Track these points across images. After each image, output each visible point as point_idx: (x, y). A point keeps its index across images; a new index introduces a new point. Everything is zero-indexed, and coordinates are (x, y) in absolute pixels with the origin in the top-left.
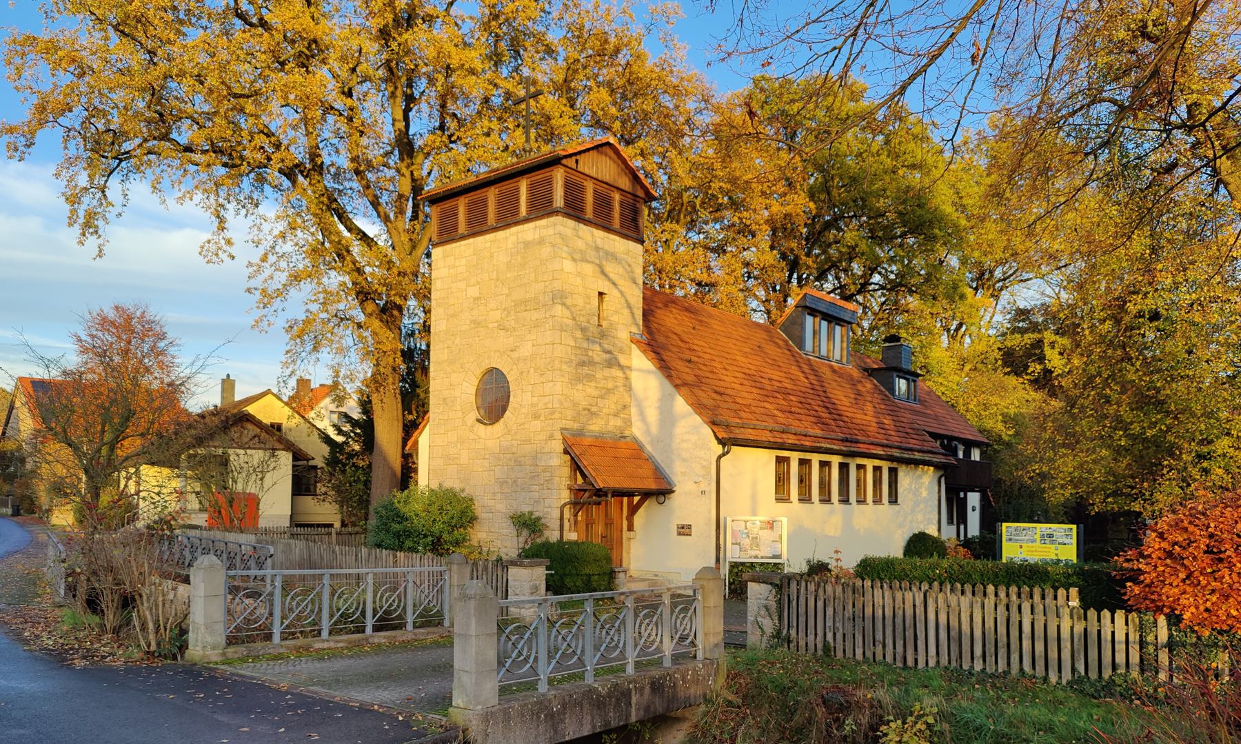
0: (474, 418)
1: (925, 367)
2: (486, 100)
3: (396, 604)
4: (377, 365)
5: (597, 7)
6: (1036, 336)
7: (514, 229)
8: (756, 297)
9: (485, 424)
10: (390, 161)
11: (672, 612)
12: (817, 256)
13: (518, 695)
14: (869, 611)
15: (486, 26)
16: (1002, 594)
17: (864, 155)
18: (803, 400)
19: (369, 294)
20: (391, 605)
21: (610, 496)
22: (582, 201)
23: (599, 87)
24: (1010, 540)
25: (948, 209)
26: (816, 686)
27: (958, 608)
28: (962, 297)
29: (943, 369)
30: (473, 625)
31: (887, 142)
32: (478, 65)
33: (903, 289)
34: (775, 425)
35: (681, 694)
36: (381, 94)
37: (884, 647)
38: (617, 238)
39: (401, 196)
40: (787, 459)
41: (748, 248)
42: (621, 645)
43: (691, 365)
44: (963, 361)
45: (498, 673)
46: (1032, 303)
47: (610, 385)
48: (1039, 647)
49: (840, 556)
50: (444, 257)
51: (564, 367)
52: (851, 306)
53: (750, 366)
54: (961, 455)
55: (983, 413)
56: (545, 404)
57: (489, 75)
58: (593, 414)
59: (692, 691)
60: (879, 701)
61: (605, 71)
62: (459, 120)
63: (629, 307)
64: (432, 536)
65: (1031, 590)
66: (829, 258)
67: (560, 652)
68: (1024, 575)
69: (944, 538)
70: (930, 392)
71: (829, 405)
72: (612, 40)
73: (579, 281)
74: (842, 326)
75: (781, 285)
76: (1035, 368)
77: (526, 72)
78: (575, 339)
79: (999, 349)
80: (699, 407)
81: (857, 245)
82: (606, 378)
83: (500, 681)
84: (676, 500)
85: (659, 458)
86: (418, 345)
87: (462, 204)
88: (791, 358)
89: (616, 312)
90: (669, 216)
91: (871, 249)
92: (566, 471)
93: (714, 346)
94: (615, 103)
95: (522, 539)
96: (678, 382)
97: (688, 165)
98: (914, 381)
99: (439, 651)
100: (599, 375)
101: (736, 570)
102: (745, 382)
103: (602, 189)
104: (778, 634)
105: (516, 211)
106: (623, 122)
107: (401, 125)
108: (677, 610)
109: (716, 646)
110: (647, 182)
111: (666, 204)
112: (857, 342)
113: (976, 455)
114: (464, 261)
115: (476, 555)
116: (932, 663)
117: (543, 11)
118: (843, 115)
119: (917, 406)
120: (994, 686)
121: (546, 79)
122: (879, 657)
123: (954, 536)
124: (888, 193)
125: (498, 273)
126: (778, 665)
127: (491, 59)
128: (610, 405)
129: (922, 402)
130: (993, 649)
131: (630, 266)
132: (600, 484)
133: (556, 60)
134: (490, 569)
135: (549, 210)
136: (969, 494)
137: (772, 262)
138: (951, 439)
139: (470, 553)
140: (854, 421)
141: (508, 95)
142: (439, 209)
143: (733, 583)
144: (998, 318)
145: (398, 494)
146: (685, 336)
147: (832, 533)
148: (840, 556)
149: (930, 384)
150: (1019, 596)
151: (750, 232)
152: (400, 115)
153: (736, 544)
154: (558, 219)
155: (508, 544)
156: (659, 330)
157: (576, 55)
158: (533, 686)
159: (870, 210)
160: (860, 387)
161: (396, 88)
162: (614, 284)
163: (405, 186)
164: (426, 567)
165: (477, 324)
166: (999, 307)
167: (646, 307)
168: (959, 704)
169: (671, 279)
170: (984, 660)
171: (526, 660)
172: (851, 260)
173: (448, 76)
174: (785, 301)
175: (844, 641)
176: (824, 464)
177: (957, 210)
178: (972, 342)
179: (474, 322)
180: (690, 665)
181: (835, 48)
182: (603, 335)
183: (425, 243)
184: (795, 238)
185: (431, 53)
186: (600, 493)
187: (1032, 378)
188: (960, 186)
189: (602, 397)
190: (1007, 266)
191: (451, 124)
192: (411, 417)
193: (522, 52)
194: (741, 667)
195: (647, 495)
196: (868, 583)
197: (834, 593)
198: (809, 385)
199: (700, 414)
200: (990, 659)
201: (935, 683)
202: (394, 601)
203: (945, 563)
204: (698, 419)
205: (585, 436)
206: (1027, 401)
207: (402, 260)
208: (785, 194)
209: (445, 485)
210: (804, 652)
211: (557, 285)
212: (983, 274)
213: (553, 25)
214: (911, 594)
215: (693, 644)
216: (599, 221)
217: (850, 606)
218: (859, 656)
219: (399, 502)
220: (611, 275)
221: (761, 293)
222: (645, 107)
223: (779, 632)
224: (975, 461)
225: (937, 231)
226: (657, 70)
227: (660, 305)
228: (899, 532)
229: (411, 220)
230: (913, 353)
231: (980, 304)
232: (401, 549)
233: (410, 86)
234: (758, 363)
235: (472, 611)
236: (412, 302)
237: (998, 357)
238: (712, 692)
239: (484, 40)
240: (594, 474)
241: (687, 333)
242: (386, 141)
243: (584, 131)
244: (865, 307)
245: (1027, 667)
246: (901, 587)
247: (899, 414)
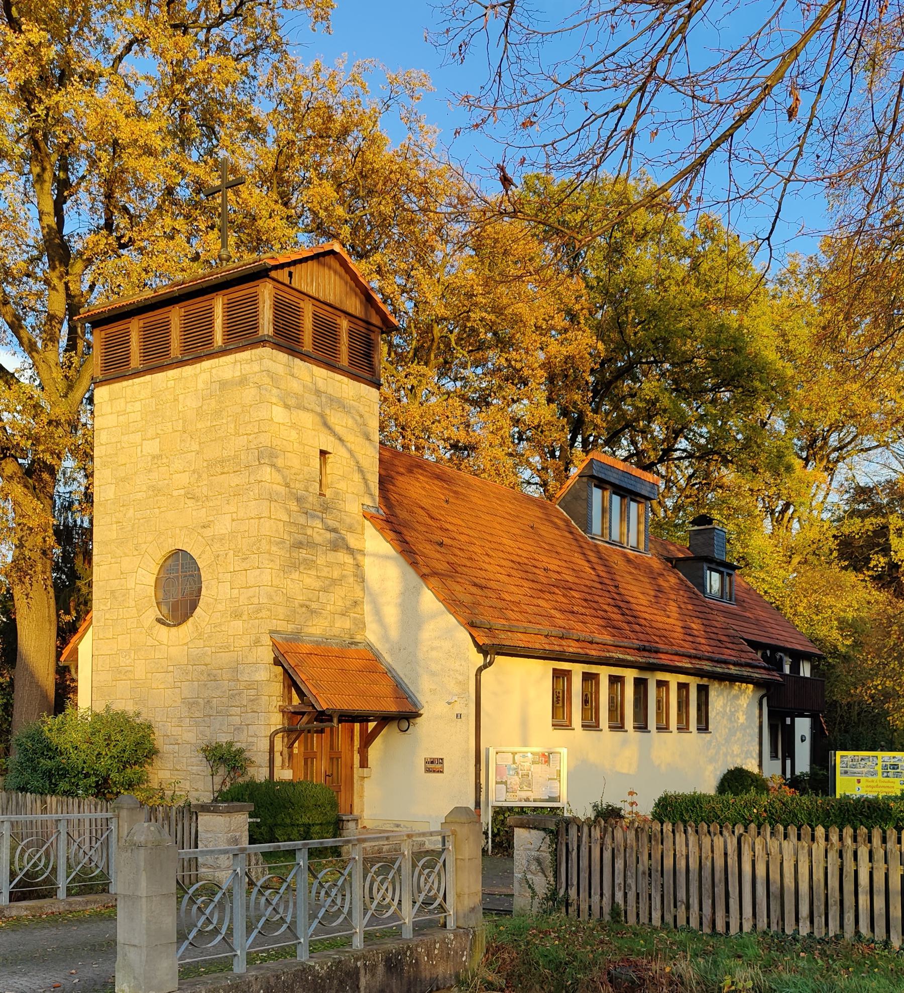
0: (153, 617)
1: (743, 558)
2: (170, 191)
3: (42, 864)
4: (20, 546)
5: (318, 71)
6: (880, 520)
7: (206, 364)
8: (529, 464)
9: (168, 625)
10: (37, 270)
11: (414, 866)
12: (607, 413)
13: (205, 978)
14: (668, 863)
15: (169, 92)
16: (834, 838)
17: (666, 283)
18: (588, 597)
19: (8, 449)
20: (35, 865)
21: (335, 720)
22: (298, 328)
23: (321, 179)
24: (846, 772)
25: (771, 355)
26: (601, 960)
27: (779, 856)
28: (789, 468)
29: (767, 561)
30: (144, 883)
31: (695, 267)
32: (157, 142)
33: (716, 457)
34: (552, 628)
35: (426, 974)
36: (24, 178)
37: (688, 908)
38: (345, 379)
39: (51, 317)
40: (567, 673)
41: (518, 400)
42: (346, 910)
43: (442, 550)
44: (791, 552)
45: (178, 949)
46: (876, 479)
47: (336, 574)
48: (879, 903)
49: (635, 798)
50: (111, 400)
51: (274, 549)
52: (649, 477)
53: (520, 552)
54: (787, 670)
55: (814, 617)
56: (249, 598)
57: (172, 157)
58: (313, 612)
59: (440, 970)
60: (680, 976)
61: (329, 159)
62: (131, 217)
63: (361, 470)
64: (96, 775)
65: (870, 832)
66: (622, 416)
67: (263, 919)
68: (861, 814)
69: (766, 775)
70: (750, 590)
71: (622, 604)
72: (339, 117)
73: (294, 434)
74: (639, 502)
75: (561, 449)
76: (879, 561)
77: (222, 154)
78: (289, 512)
79: (834, 536)
80: (452, 604)
81: (657, 400)
82: (329, 565)
83: (181, 959)
84: (422, 725)
85: (401, 671)
86: (79, 522)
87: (135, 328)
88: (574, 543)
89: (344, 477)
90: (415, 355)
91: (675, 405)
92: (277, 687)
93: (473, 526)
94: (342, 201)
95: (218, 779)
96: (426, 571)
97: (440, 289)
98: (730, 575)
99: (101, 924)
100: (321, 561)
101: (501, 817)
102: (513, 572)
103: (324, 312)
104: (552, 896)
105: (209, 339)
106: (355, 230)
107: (51, 220)
108: (420, 864)
109: (473, 910)
110: (387, 309)
111: (412, 340)
112: (659, 525)
113: (806, 670)
114: (138, 406)
115: (155, 801)
116: (747, 927)
117: (244, 72)
118: (639, 229)
119: (734, 607)
120: (823, 953)
121: (250, 167)
122: (682, 921)
123: (780, 772)
124: (697, 333)
125: (185, 421)
126: (553, 935)
127: (175, 135)
128: (335, 600)
129: (739, 602)
130: (823, 907)
131: (361, 416)
132: (323, 705)
133: (264, 141)
134: (173, 818)
135: (254, 338)
136: (796, 719)
137: (549, 418)
138: (775, 649)
139: (148, 798)
140: (654, 624)
141: (199, 187)
142: (103, 334)
143: (498, 834)
144: (834, 497)
145: (50, 720)
146: (435, 512)
147: (625, 771)
148: (635, 798)
149: (749, 580)
150: (855, 840)
151: (520, 378)
152: (49, 207)
153: (501, 783)
154: (266, 352)
155: (200, 785)
156: (400, 504)
157: (290, 136)
158: (226, 965)
159: (674, 354)
160: (661, 581)
161: (44, 169)
162: (340, 439)
163: (58, 304)
164: (87, 814)
165: (156, 490)
166: (835, 484)
167: (383, 473)
168: (780, 976)
169: (418, 438)
170: (812, 922)
171: (216, 931)
172: (650, 419)
173: (115, 156)
174: (567, 469)
175: (638, 903)
176: (615, 680)
177: (782, 357)
178: (802, 527)
179: (153, 488)
180: (439, 935)
181: (617, 107)
182: (326, 508)
183: (85, 382)
184: (579, 388)
185: (91, 122)
186: (323, 716)
187: (875, 574)
188: (786, 326)
189: (325, 590)
190: (845, 431)
191: (121, 221)
192: (68, 618)
193: (217, 128)
194: (505, 938)
195: (385, 720)
196: (667, 827)
197: (625, 841)
198: (596, 578)
199: (454, 613)
200: (819, 920)
201: (750, 952)
202: (40, 859)
203: (764, 800)
204: (452, 619)
205: (303, 641)
206: (869, 603)
207: (53, 404)
208: (566, 330)
209: (113, 707)
210: (587, 918)
211: (265, 440)
212: (815, 441)
213: (259, 94)
214: (722, 839)
215: (442, 909)
216: (319, 355)
217: (646, 857)
218: (657, 921)
219: (50, 730)
220: (338, 429)
221: (536, 460)
222: (382, 208)
223: (555, 892)
225: (757, 384)
226: (399, 160)
227: (402, 470)
228: (710, 768)
229: (66, 351)
230: (728, 541)
231: (811, 479)
232: (53, 792)
233: (64, 167)
234: (530, 548)
235: (142, 864)
236: (69, 463)
237: (833, 547)
238: (467, 971)
239: (165, 109)
240: (314, 692)
241: (437, 507)
242: (31, 242)
243: (303, 238)
244: (668, 481)
245: (864, 930)
246: (709, 832)
247: (710, 617)
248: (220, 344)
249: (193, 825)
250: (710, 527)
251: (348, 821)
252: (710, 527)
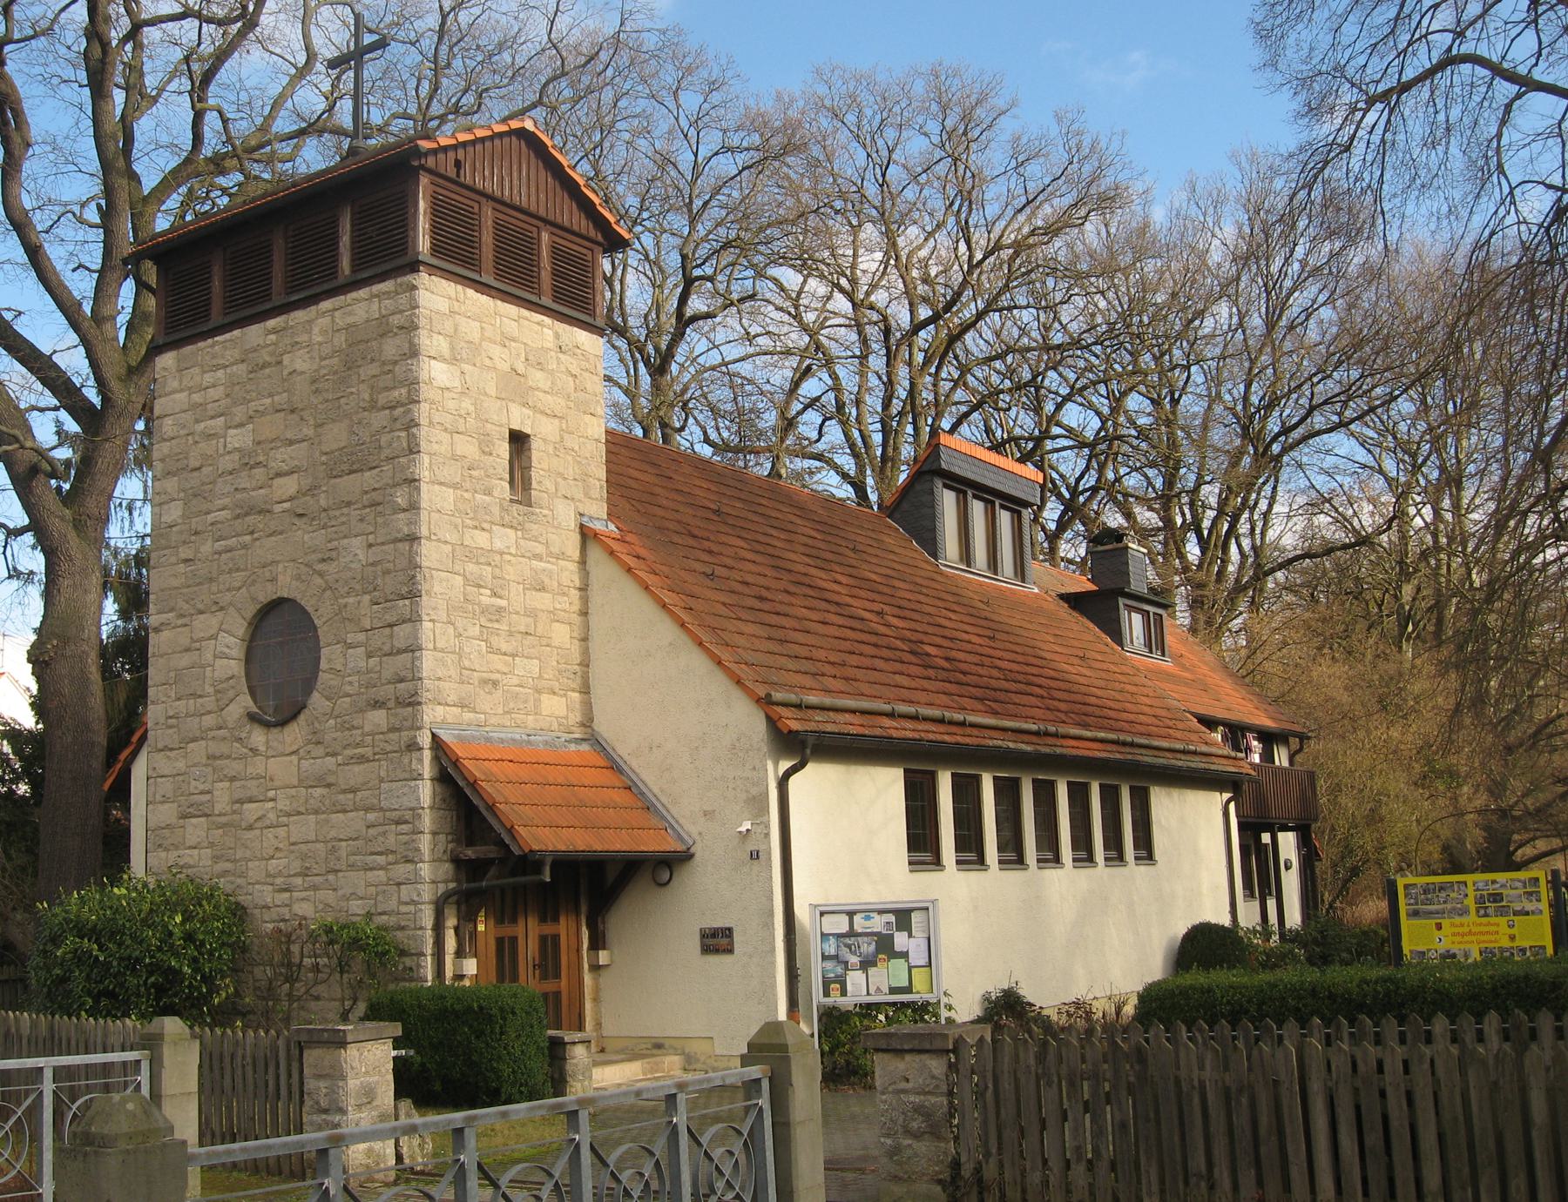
113: (1281, 758)
130: (1466, 1170)
224: (1281, 768)
248: (347, 272)
249: (295, 1065)
250: (1120, 545)
251: (574, 1043)
252: (1120, 545)
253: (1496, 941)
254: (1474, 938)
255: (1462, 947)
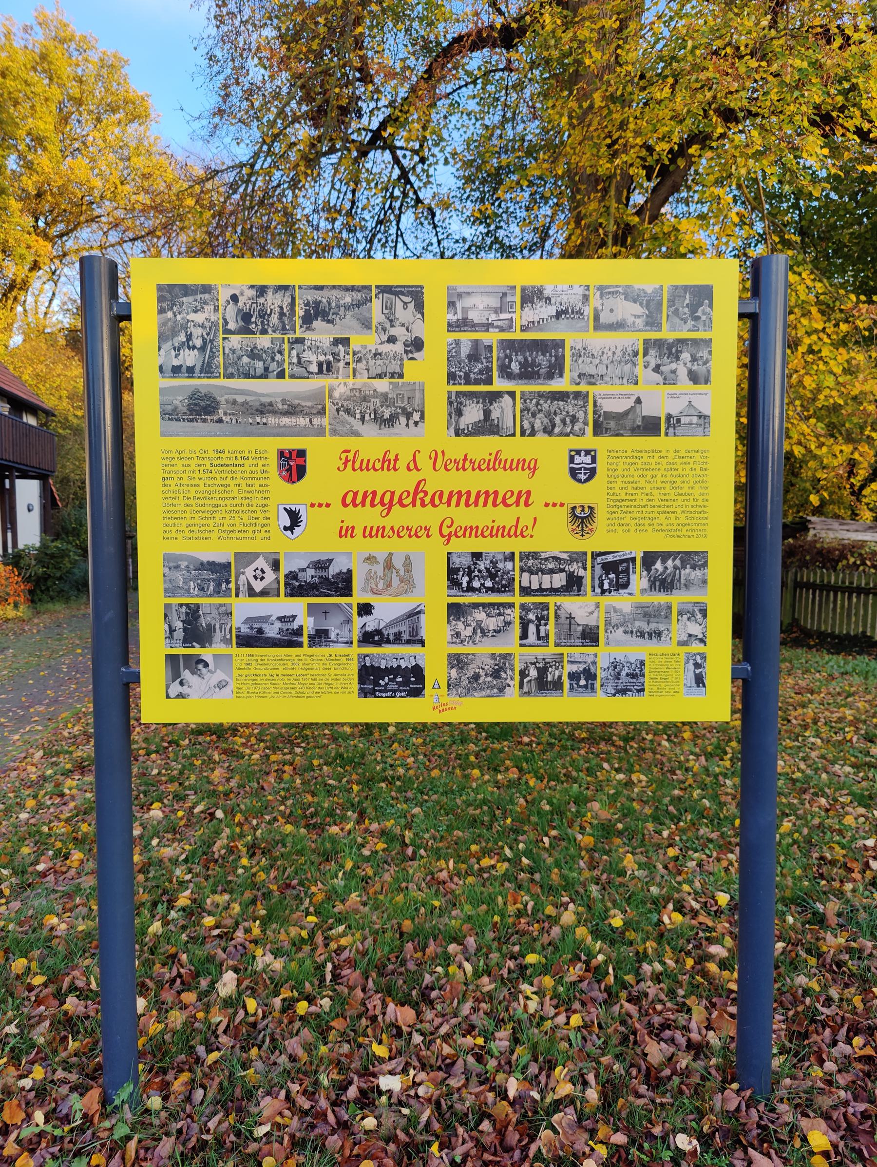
136: (18, 482)
253: (517, 532)
254: (430, 516)
255: (380, 547)
